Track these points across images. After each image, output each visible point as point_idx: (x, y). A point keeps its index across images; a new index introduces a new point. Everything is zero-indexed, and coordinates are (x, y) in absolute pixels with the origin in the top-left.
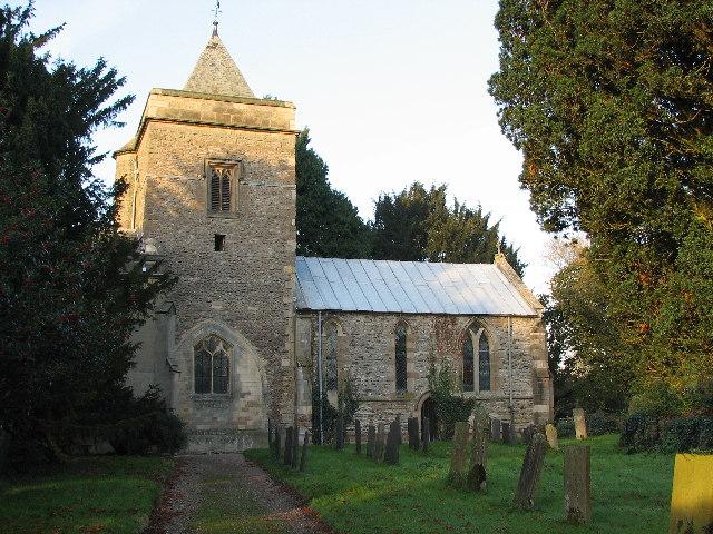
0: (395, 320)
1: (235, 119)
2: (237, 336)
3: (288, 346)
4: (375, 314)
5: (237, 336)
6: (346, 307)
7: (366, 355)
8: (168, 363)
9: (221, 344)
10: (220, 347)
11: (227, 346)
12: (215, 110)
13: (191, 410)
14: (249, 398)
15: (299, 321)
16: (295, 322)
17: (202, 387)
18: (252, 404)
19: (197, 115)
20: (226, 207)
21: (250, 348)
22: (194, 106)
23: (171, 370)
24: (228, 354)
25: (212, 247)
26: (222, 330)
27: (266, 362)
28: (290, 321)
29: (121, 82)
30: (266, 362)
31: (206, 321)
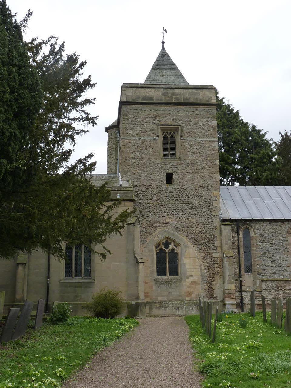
0: (244, 241)
1: (176, 99)
2: (182, 238)
3: (217, 244)
4: (276, 221)
5: (182, 238)
6: (254, 217)
7: (271, 249)
8: (135, 257)
9: (172, 243)
10: (172, 246)
11: (177, 245)
12: (163, 94)
13: (154, 287)
14: (192, 279)
15: (223, 227)
16: (221, 227)
17: (161, 272)
18: (194, 283)
19: (151, 98)
20: (174, 155)
21: (190, 244)
22: (150, 93)
23: (137, 261)
24: (177, 250)
25: (164, 183)
26: (173, 234)
27: (203, 255)
28: (218, 227)
29: (83, 65)
30: (203, 255)
31: (163, 229)
